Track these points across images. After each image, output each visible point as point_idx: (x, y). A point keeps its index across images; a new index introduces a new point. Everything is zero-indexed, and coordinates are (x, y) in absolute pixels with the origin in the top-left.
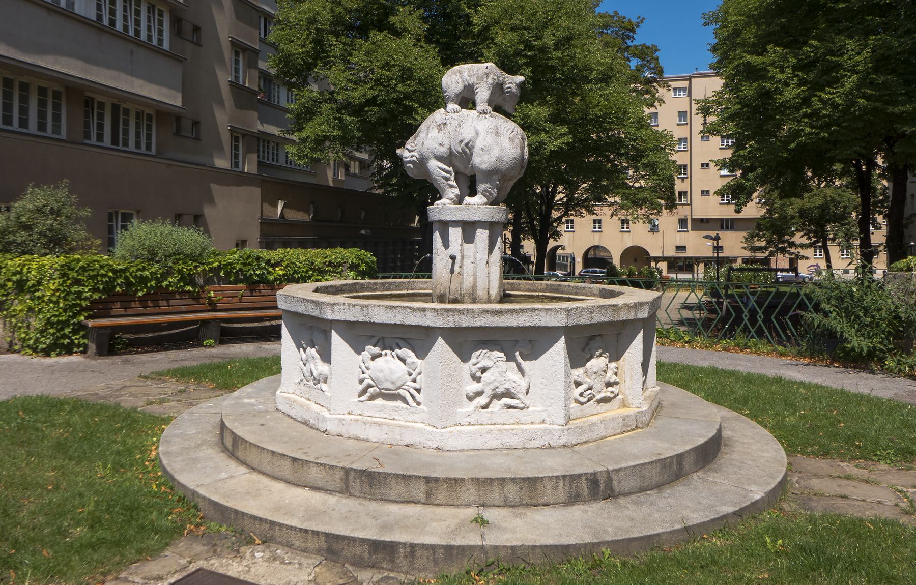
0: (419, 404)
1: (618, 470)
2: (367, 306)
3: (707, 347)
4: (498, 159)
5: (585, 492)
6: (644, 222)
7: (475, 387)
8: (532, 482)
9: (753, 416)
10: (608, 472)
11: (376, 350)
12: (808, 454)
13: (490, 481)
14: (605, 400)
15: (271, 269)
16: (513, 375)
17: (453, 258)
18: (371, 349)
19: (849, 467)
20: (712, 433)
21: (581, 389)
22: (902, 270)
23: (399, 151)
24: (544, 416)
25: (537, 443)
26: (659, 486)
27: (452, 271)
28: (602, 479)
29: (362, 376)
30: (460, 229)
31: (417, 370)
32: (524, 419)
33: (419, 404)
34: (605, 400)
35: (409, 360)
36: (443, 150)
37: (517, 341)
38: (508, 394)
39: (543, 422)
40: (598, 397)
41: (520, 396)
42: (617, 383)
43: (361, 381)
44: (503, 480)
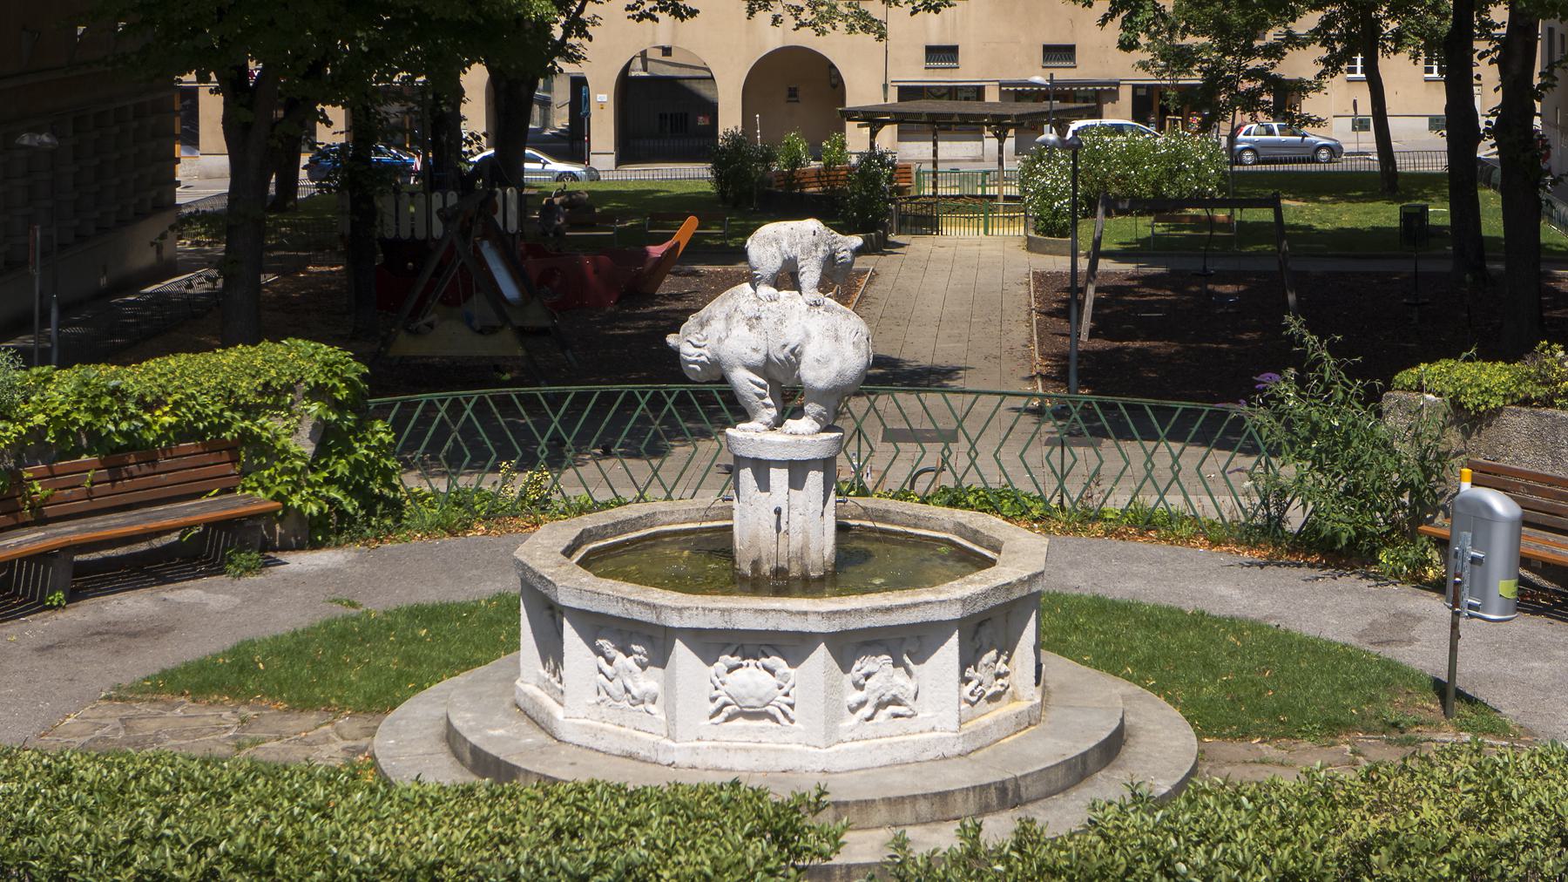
0: (792, 721)
1: (1025, 776)
2: (729, 611)
3: (1075, 530)
4: (840, 374)
5: (995, 802)
6: (851, 29)
7: (858, 696)
8: (943, 797)
9: (1159, 689)
10: (1016, 778)
11: (736, 660)
12: (1225, 737)
13: (902, 799)
14: (995, 697)
15: (147, 417)
16: (899, 676)
17: (778, 512)
18: (726, 660)
19: (1269, 750)
20: (1114, 726)
21: (972, 685)
22: (1410, 389)
23: (671, 339)
24: (934, 722)
25: (930, 755)
26: (1064, 790)
27: (778, 529)
28: (1010, 787)
29: (715, 693)
30: (786, 471)
31: (791, 682)
32: (912, 729)
33: (792, 721)
34: (995, 697)
35: (779, 671)
36: (758, 358)
37: (903, 639)
38: (895, 701)
39: (933, 729)
40: (988, 693)
41: (909, 702)
42: (1007, 674)
43: (713, 700)
44: (915, 797)
